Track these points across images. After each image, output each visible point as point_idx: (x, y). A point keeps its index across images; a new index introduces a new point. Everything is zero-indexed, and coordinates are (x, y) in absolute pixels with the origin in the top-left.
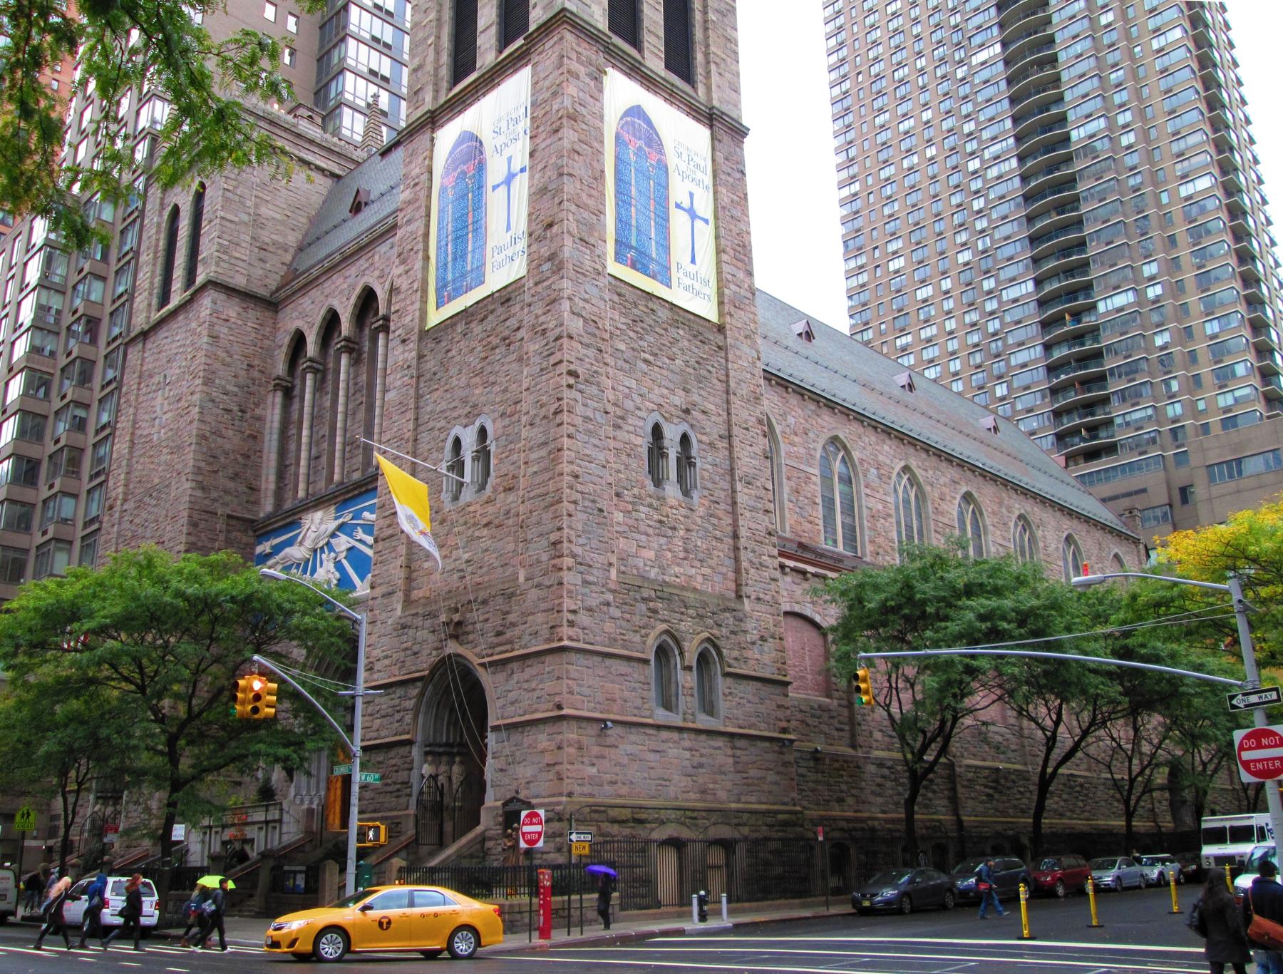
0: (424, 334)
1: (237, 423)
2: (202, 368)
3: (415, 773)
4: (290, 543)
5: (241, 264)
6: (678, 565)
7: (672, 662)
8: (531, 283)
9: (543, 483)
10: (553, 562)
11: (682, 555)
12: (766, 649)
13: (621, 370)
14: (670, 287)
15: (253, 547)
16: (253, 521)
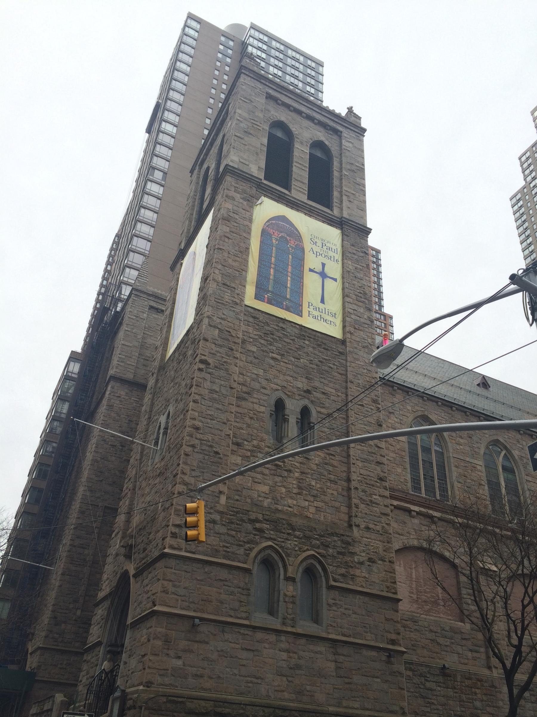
6: (291, 498)
7: (277, 573)
11: (295, 491)
12: (375, 569)
13: (251, 363)
14: (301, 316)
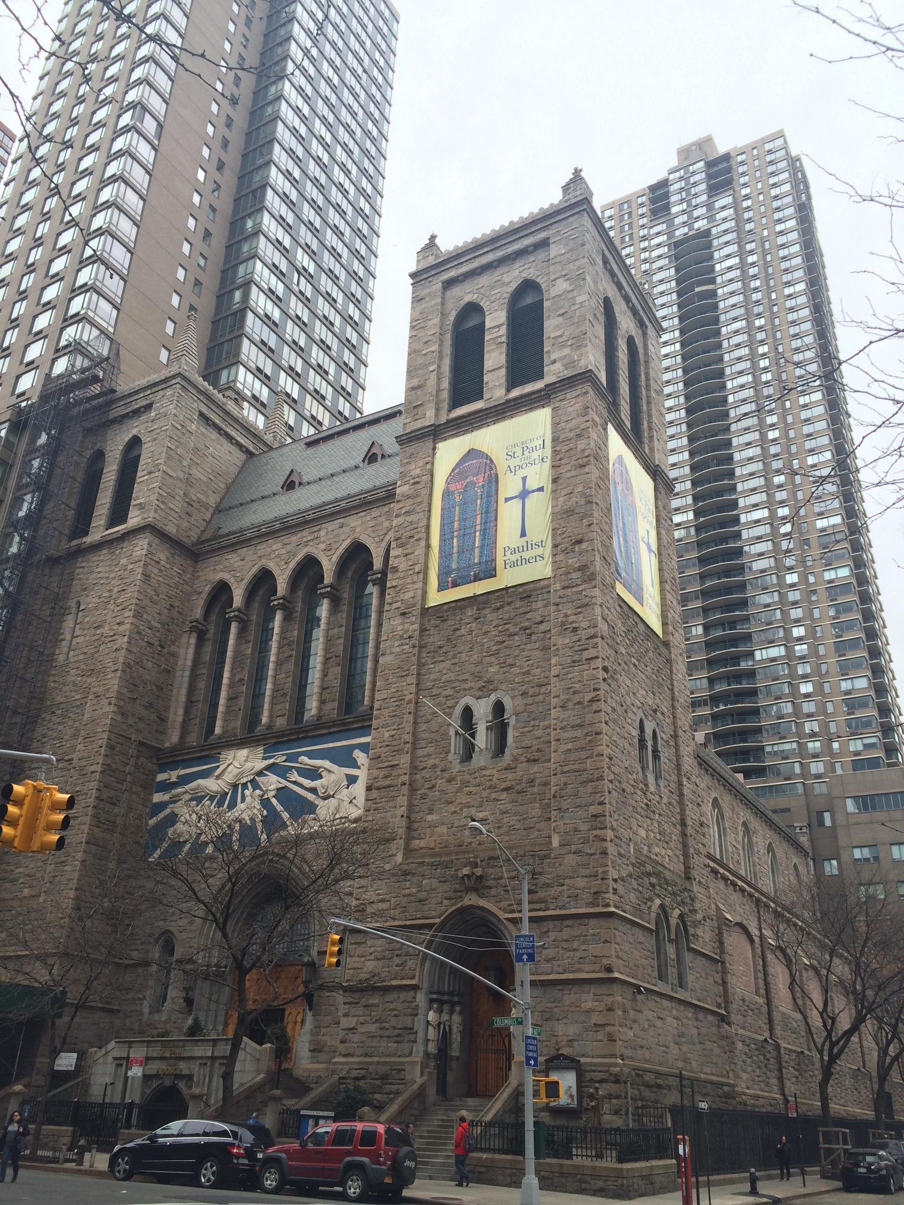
0: (426, 611)
1: (156, 656)
2: (134, 601)
3: (420, 1019)
4: (205, 775)
5: (173, 513)
8: (558, 586)
9: (582, 761)
10: (595, 832)
15: (154, 774)
16: (160, 750)
